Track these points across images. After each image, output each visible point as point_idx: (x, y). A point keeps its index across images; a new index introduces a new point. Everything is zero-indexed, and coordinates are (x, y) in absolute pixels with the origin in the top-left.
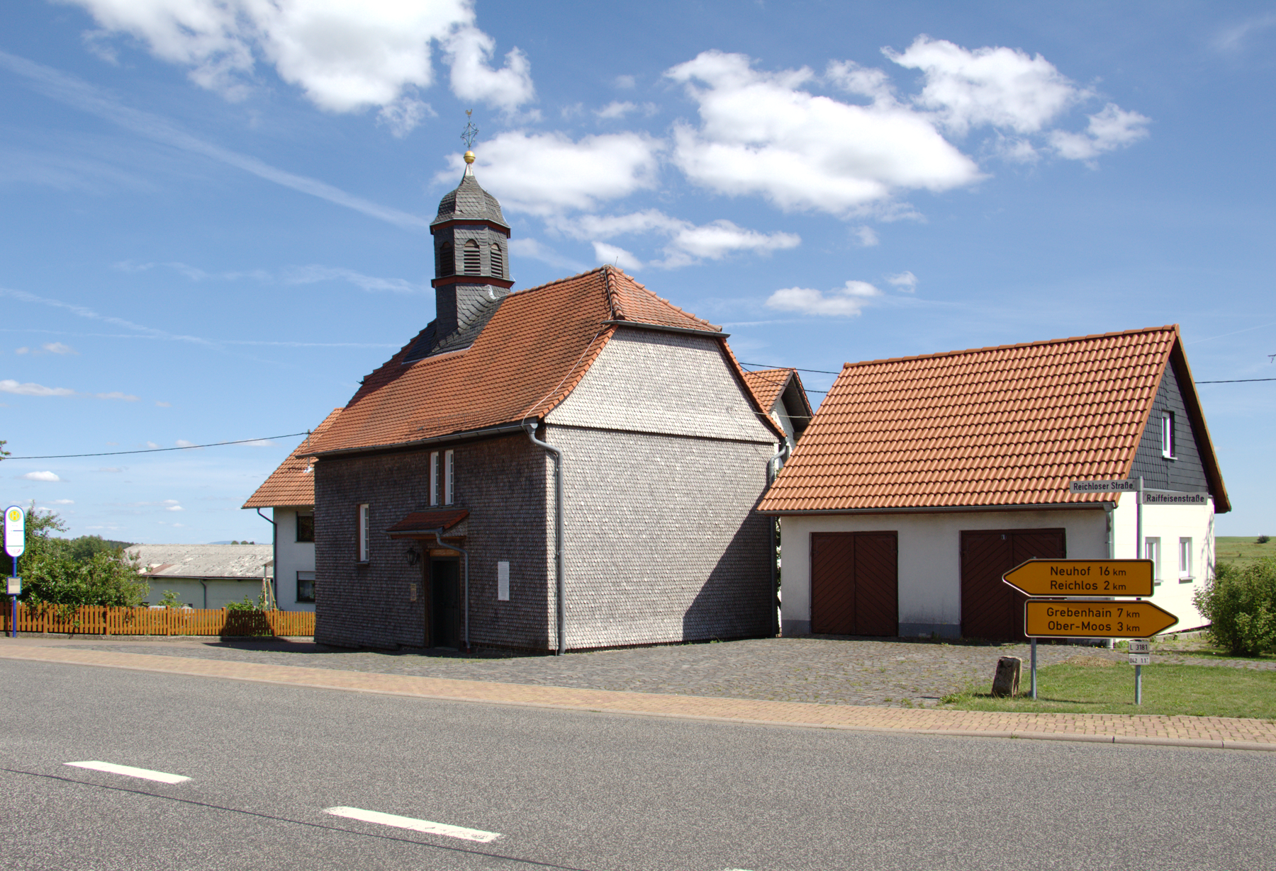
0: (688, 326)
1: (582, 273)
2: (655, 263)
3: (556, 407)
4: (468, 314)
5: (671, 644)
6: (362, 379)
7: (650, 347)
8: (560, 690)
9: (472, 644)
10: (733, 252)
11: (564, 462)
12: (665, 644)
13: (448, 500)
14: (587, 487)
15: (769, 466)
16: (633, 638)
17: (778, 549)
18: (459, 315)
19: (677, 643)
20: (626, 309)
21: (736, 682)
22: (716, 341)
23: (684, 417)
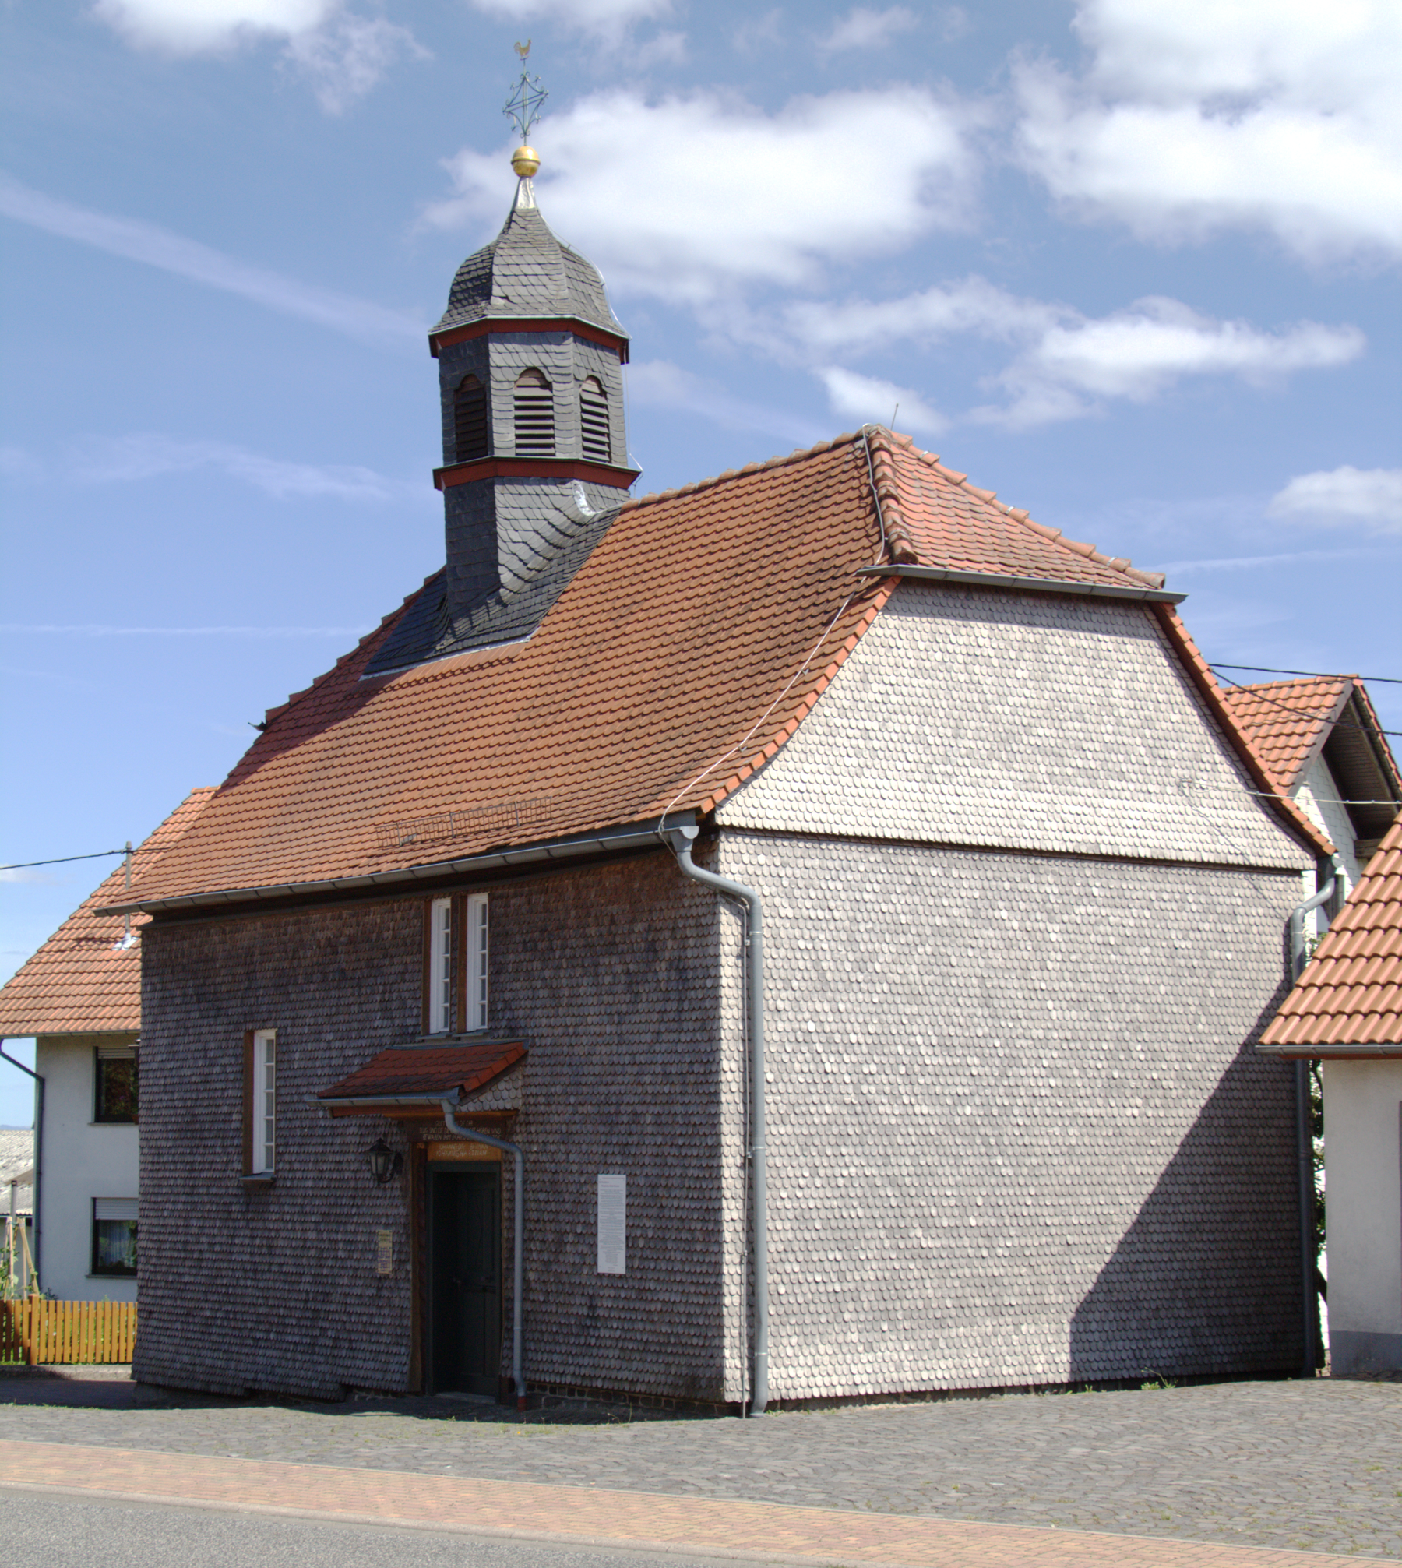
0: (1078, 575)
1: (809, 446)
2: (984, 415)
3: (744, 784)
4: (524, 552)
5: (1039, 1388)
6: (262, 719)
7: (981, 630)
8: (752, 1509)
9: (531, 1386)
10: (1186, 385)
11: (766, 923)
12: (1025, 1389)
13: (474, 1019)
14: (823, 986)
15: (1290, 930)
16: (941, 1373)
17: (1318, 1143)
18: (502, 557)
19: (1056, 1388)
20: (920, 534)
21: (1210, 1498)
22: (1152, 612)
23: (1067, 805)
